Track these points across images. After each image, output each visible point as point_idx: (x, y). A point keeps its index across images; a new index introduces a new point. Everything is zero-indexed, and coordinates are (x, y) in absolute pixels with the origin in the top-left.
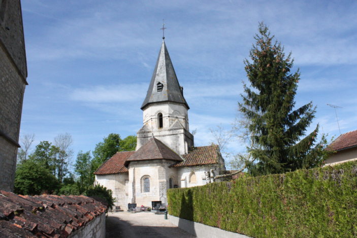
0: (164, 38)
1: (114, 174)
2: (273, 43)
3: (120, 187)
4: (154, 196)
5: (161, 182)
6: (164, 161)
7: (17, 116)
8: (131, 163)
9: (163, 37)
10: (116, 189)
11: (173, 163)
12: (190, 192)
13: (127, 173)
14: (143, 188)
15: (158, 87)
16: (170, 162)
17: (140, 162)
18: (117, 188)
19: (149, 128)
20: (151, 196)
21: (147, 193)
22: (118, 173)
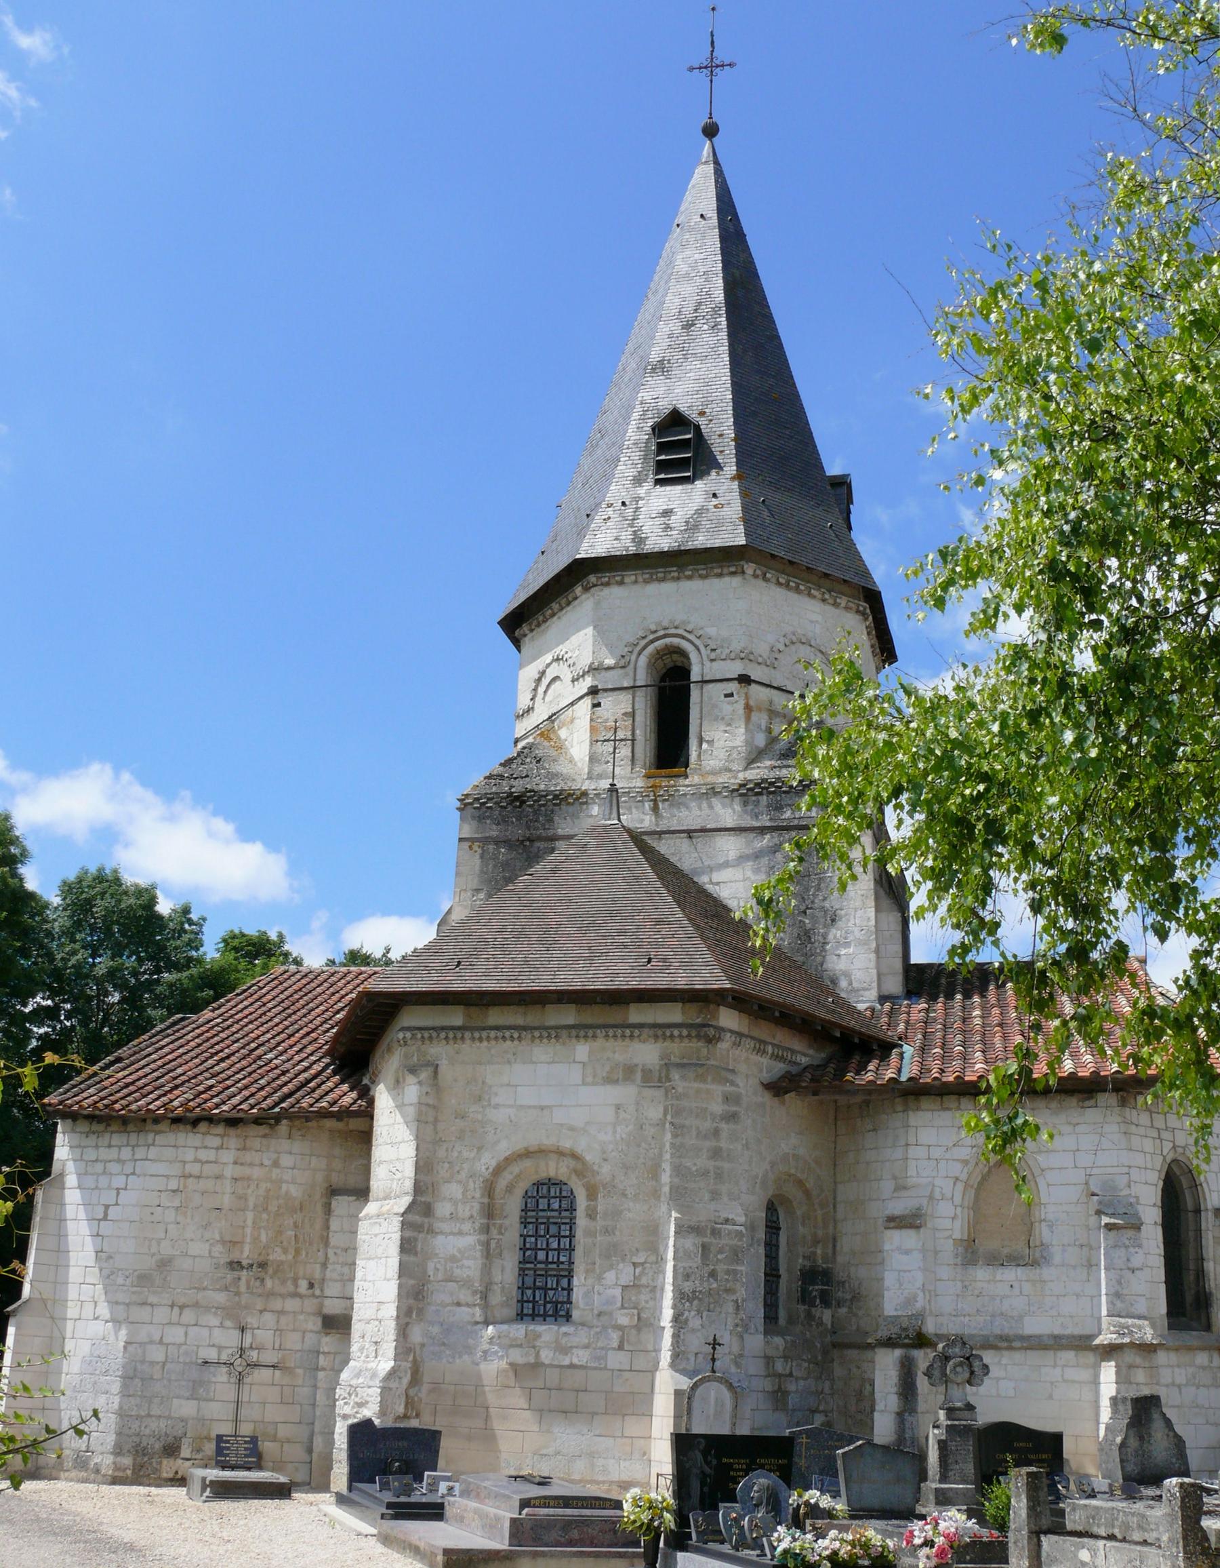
0: (711, 131)
1: (232, 1123)
2: (843, 912)
3: (166, 1249)
4: (616, 1360)
5: (696, 1230)
6: (728, 1018)
7: (272, 1121)
8: (410, 1018)
9: (705, 120)
10: (235, 1265)
11: (805, 1054)
12: (38, 1164)
13: (357, 1129)
14: (507, 1272)
15: (662, 448)
16: (782, 1037)
17: (496, 1016)
18: (246, 1254)
19: (563, 768)
20: (580, 1357)
21: (547, 1332)
22: (266, 1120)
